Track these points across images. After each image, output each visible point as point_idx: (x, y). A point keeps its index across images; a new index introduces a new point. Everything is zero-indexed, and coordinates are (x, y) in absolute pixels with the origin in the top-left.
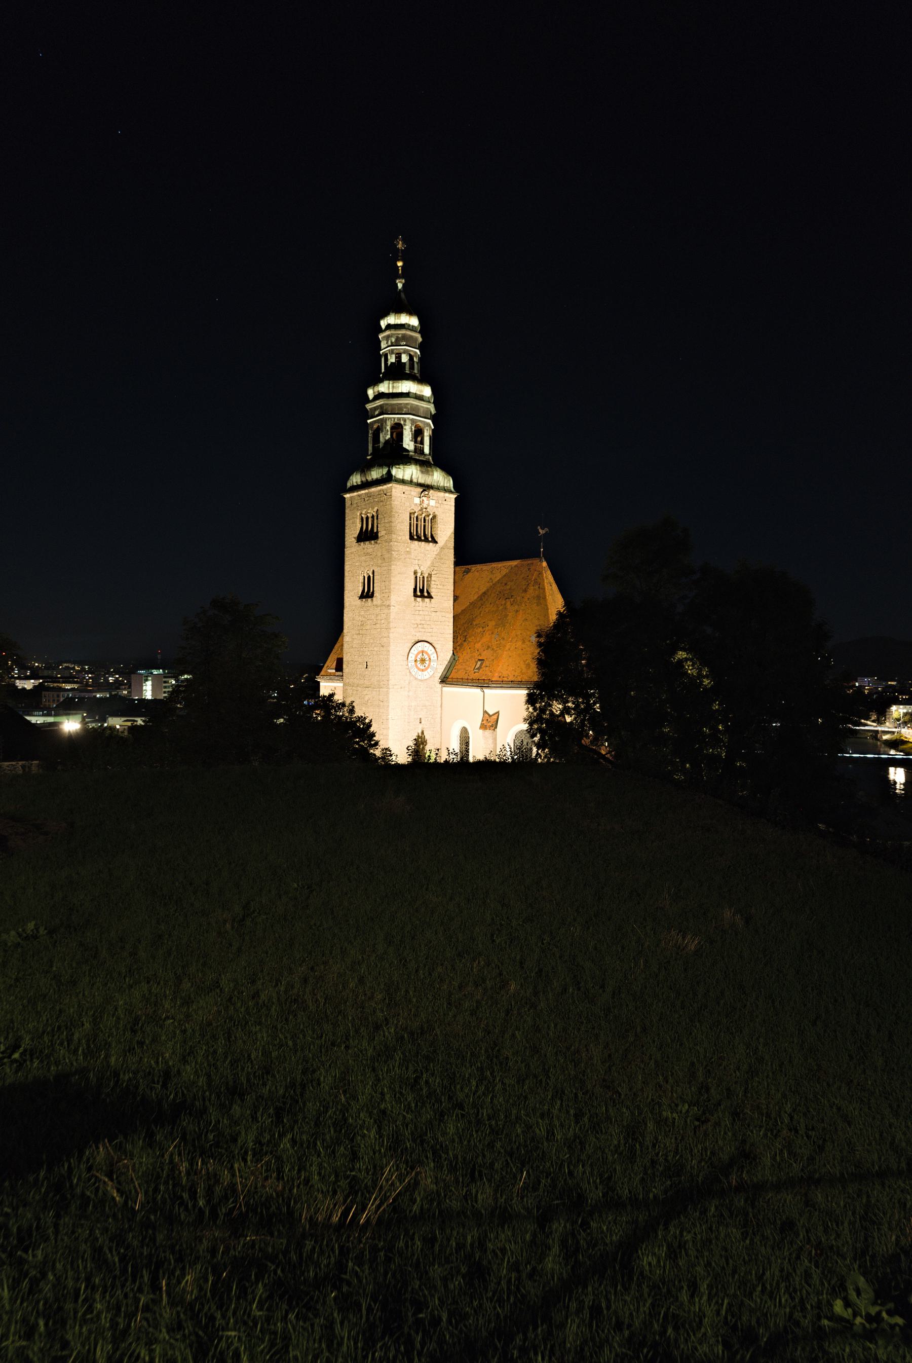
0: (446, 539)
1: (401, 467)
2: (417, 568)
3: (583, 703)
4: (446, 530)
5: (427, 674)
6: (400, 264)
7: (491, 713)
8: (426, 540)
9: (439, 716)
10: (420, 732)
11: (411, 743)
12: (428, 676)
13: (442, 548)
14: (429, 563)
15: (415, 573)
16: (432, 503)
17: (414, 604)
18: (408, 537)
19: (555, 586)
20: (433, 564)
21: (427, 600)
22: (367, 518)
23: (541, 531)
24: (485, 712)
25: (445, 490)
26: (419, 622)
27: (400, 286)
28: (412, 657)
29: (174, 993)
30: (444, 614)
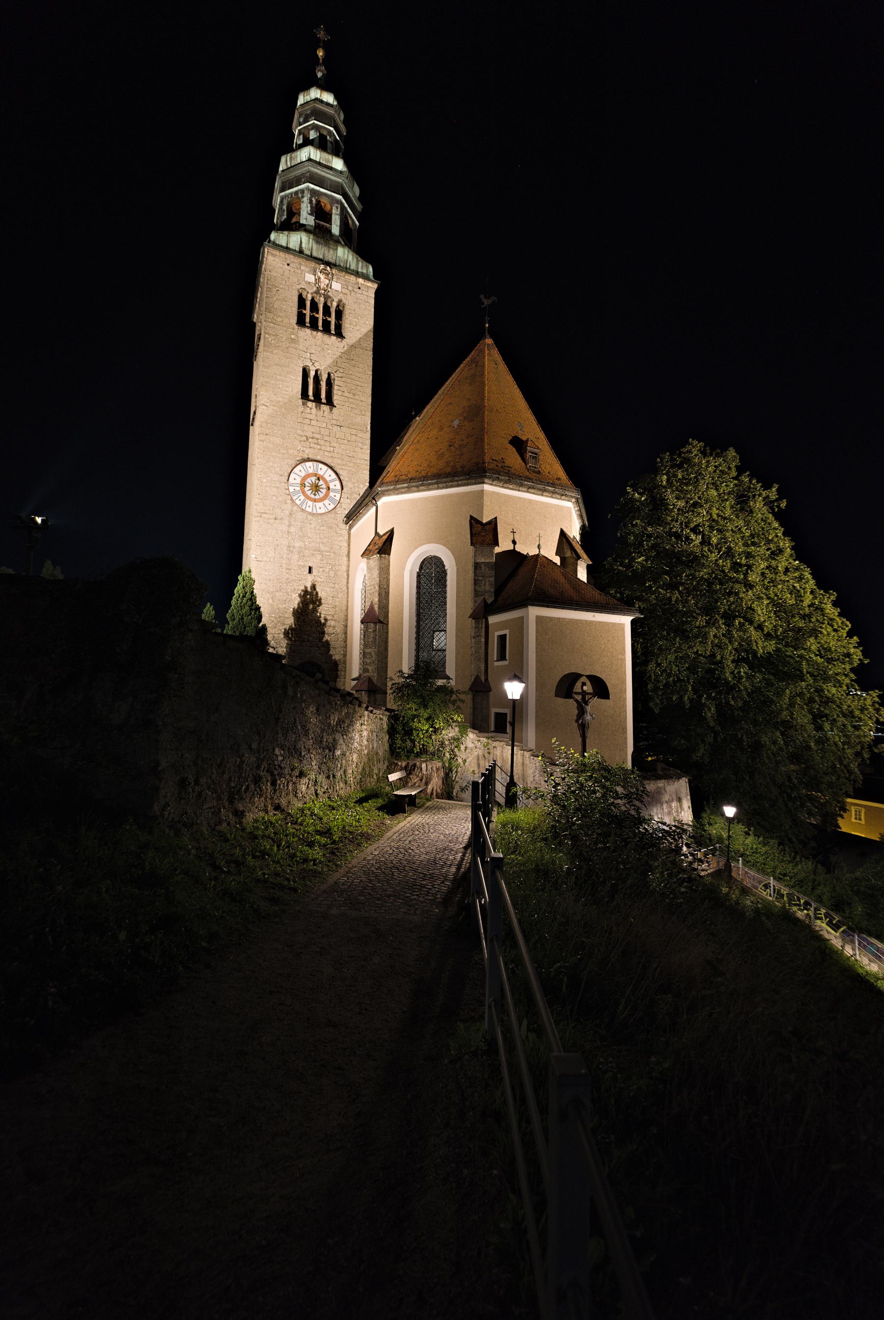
0: (359, 336)
1: (286, 233)
2: (309, 364)
3: (616, 592)
4: (361, 321)
5: (321, 508)
6: (320, 53)
7: (381, 534)
8: (326, 330)
9: (345, 568)
10: (309, 585)
13: (352, 347)
14: (329, 361)
15: (305, 373)
16: (336, 286)
17: (301, 409)
18: (294, 320)
21: (325, 408)
22: (317, 378)
24: (376, 533)
25: (365, 277)
26: (310, 434)
27: (320, 75)
28: (296, 479)
29: (265, 881)
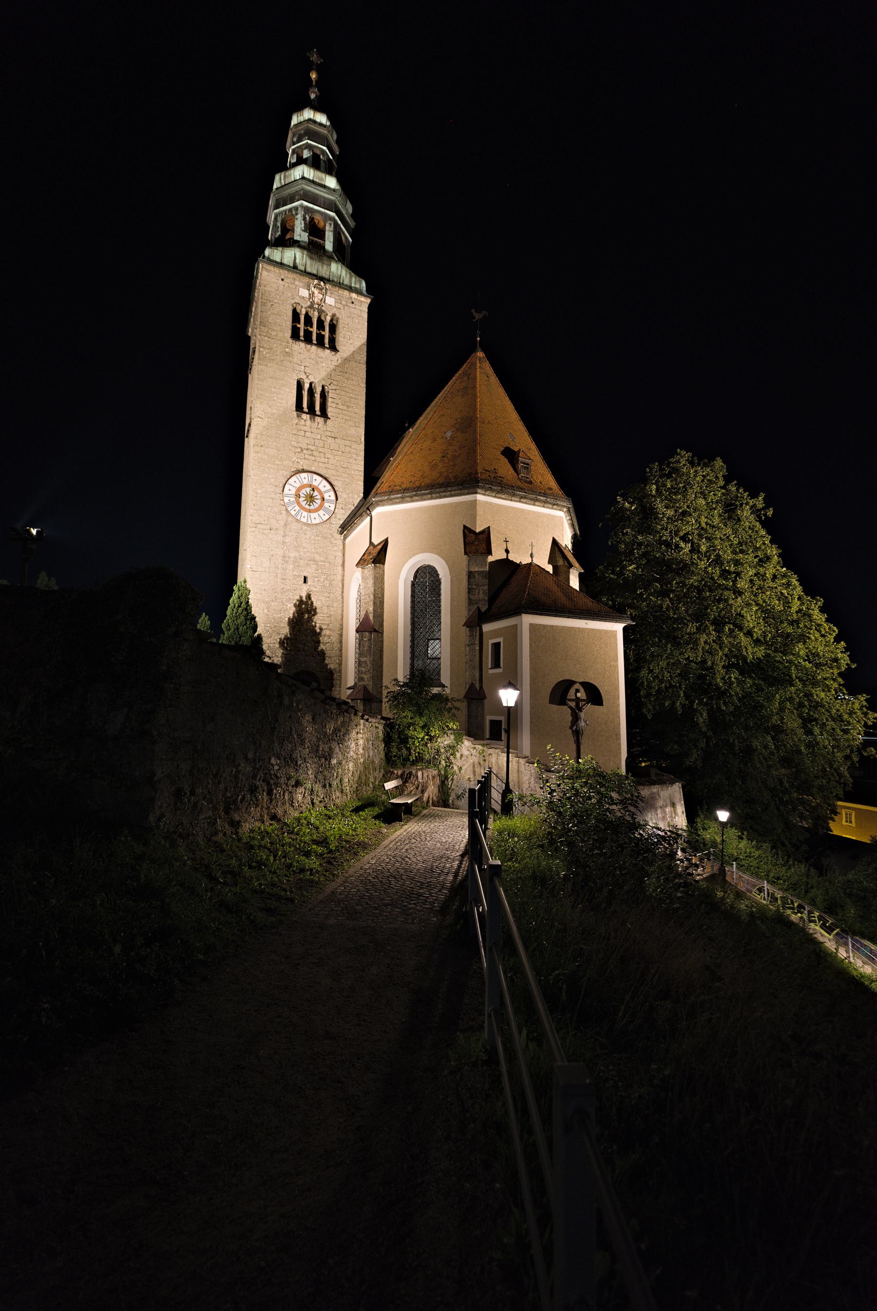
0: (352, 349)
2: (303, 376)
4: (354, 334)
6: (314, 76)
8: (320, 343)
9: (339, 578)
10: (304, 595)
11: (291, 611)
12: (317, 521)
13: (346, 360)
15: (300, 385)
17: (296, 421)
18: (289, 333)
19: (494, 380)
20: (329, 376)
21: (320, 420)
22: (311, 391)
23: (475, 314)
24: (371, 543)
25: (359, 292)
26: (304, 446)
27: (313, 96)
28: (290, 490)
30: (348, 443)
